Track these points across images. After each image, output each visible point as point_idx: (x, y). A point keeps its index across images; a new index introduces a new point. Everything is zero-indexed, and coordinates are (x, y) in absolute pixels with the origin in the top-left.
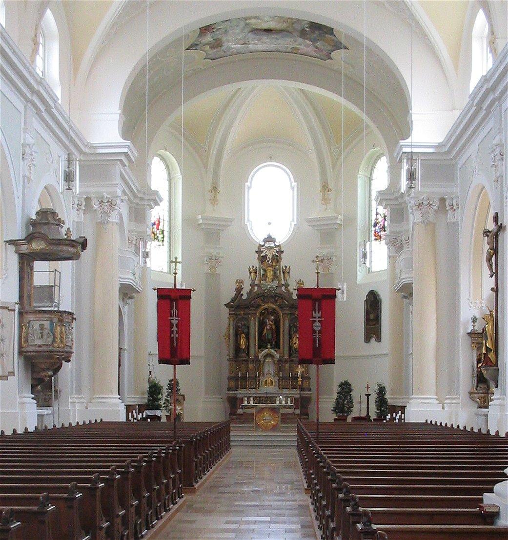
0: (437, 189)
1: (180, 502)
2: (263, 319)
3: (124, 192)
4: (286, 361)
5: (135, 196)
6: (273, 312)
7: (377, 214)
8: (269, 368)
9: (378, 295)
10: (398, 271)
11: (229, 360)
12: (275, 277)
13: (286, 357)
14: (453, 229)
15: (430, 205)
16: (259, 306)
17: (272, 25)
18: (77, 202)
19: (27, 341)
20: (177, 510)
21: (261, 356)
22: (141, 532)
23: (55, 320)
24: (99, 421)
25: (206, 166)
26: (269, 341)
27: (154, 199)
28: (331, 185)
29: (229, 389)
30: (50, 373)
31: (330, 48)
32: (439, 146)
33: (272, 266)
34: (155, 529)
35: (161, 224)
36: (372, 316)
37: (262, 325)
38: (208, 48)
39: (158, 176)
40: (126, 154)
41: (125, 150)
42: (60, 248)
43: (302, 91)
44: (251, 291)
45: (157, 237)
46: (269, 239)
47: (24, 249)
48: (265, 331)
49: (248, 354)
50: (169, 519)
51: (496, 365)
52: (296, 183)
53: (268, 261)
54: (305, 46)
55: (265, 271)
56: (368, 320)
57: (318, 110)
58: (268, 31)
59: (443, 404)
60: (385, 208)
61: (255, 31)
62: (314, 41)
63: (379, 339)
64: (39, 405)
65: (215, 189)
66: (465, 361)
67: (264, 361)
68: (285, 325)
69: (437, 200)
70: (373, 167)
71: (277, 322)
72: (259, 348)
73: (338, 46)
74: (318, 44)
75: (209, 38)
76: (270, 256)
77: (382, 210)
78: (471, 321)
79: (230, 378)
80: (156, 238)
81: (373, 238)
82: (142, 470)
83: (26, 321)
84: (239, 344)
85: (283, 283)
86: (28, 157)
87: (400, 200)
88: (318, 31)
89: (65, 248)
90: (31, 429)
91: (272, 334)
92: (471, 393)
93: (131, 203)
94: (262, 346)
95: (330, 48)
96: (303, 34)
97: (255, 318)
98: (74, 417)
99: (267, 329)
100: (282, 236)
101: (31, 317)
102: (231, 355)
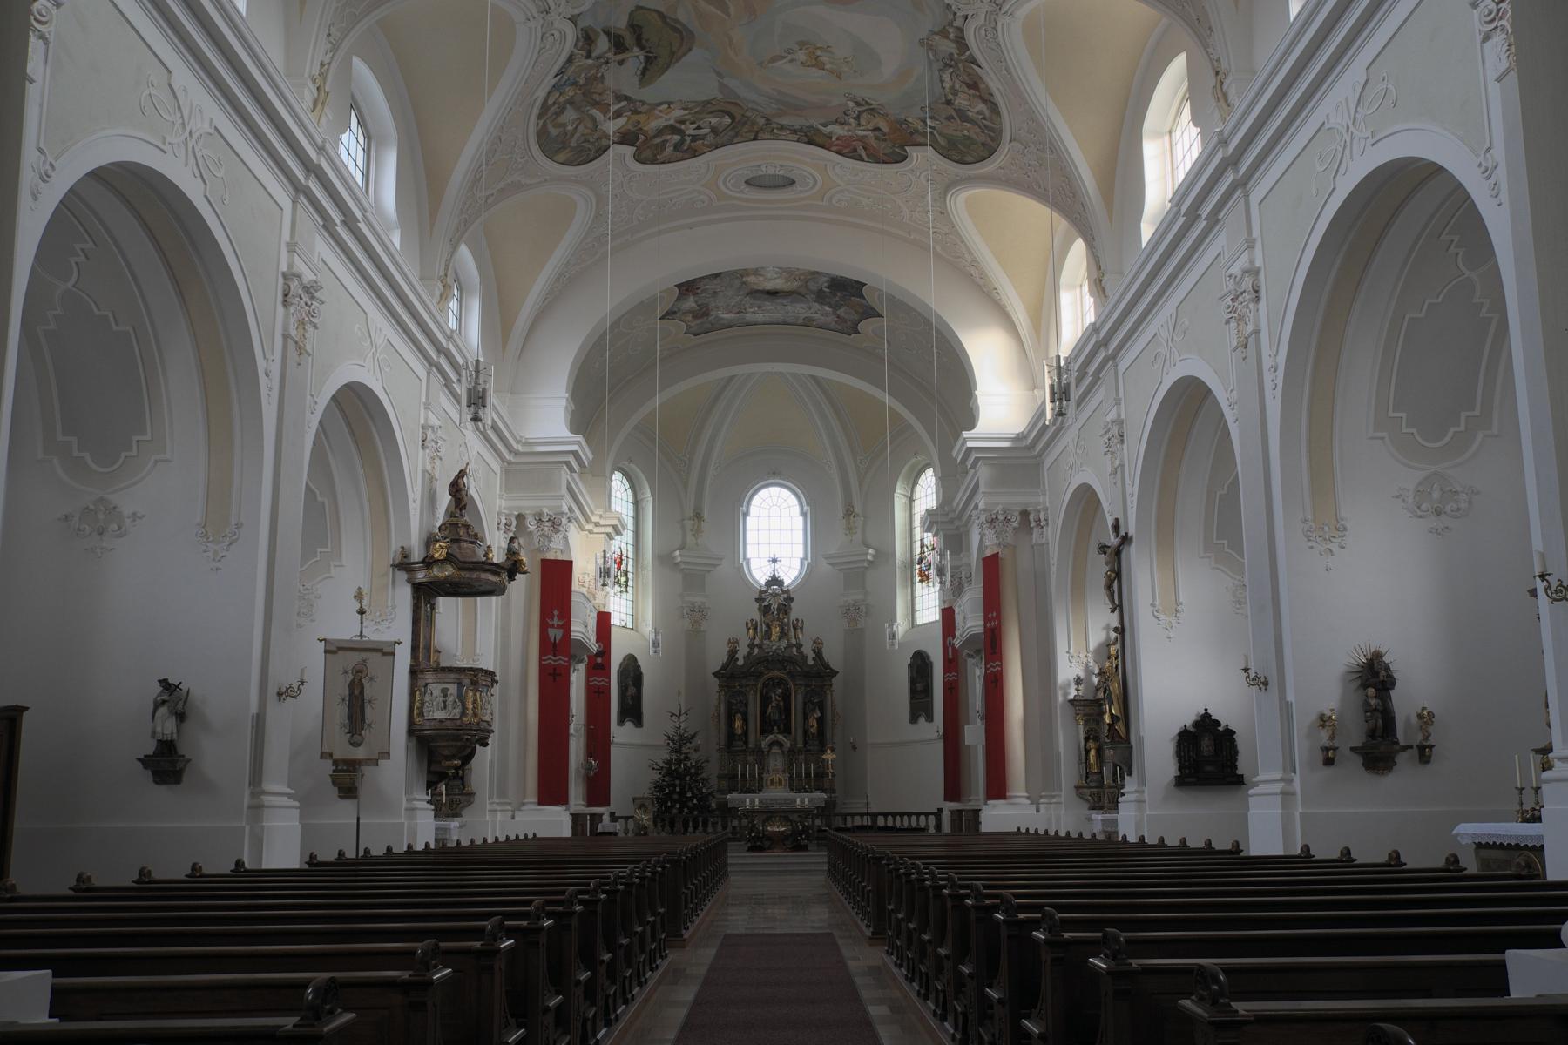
0: (1016, 499)
1: (663, 965)
4: (800, 751)
6: (780, 682)
7: (922, 546)
8: (776, 762)
11: (719, 751)
12: (783, 634)
13: (800, 745)
15: (1007, 520)
16: (761, 675)
17: (778, 284)
19: (421, 714)
20: (659, 983)
21: (764, 744)
22: (595, 1035)
23: (466, 682)
28: (858, 509)
31: (856, 317)
34: (620, 1026)
36: (919, 686)
37: (765, 701)
38: (689, 317)
40: (575, 454)
41: (575, 448)
42: (475, 575)
43: (814, 378)
44: (749, 654)
46: (774, 581)
47: (421, 576)
49: (746, 743)
50: (646, 1000)
51: (1128, 740)
54: (822, 313)
55: (768, 626)
56: (913, 692)
58: (773, 294)
59: (1038, 805)
61: (756, 293)
62: (835, 307)
64: (438, 814)
65: (698, 516)
66: (1067, 737)
68: (797, 701)
70: (915, 483)
71: (786, 697)
73: (870, 313)
74: (841, 312)
75: (690, 303)
76: (775, 605)
77: (929, 538)
80: (618, 583)
82: (599, 909)
83: (421, 683)
87: (957, 523)
88: (845, 296)
89: (484, 576)
90: (420, 847)
92: (1077, 788)
94: (766, 727)
95: (856, 317)
96: (820, 297)
98: (494, 830)
100: (790, 574)
101: (429, 677)
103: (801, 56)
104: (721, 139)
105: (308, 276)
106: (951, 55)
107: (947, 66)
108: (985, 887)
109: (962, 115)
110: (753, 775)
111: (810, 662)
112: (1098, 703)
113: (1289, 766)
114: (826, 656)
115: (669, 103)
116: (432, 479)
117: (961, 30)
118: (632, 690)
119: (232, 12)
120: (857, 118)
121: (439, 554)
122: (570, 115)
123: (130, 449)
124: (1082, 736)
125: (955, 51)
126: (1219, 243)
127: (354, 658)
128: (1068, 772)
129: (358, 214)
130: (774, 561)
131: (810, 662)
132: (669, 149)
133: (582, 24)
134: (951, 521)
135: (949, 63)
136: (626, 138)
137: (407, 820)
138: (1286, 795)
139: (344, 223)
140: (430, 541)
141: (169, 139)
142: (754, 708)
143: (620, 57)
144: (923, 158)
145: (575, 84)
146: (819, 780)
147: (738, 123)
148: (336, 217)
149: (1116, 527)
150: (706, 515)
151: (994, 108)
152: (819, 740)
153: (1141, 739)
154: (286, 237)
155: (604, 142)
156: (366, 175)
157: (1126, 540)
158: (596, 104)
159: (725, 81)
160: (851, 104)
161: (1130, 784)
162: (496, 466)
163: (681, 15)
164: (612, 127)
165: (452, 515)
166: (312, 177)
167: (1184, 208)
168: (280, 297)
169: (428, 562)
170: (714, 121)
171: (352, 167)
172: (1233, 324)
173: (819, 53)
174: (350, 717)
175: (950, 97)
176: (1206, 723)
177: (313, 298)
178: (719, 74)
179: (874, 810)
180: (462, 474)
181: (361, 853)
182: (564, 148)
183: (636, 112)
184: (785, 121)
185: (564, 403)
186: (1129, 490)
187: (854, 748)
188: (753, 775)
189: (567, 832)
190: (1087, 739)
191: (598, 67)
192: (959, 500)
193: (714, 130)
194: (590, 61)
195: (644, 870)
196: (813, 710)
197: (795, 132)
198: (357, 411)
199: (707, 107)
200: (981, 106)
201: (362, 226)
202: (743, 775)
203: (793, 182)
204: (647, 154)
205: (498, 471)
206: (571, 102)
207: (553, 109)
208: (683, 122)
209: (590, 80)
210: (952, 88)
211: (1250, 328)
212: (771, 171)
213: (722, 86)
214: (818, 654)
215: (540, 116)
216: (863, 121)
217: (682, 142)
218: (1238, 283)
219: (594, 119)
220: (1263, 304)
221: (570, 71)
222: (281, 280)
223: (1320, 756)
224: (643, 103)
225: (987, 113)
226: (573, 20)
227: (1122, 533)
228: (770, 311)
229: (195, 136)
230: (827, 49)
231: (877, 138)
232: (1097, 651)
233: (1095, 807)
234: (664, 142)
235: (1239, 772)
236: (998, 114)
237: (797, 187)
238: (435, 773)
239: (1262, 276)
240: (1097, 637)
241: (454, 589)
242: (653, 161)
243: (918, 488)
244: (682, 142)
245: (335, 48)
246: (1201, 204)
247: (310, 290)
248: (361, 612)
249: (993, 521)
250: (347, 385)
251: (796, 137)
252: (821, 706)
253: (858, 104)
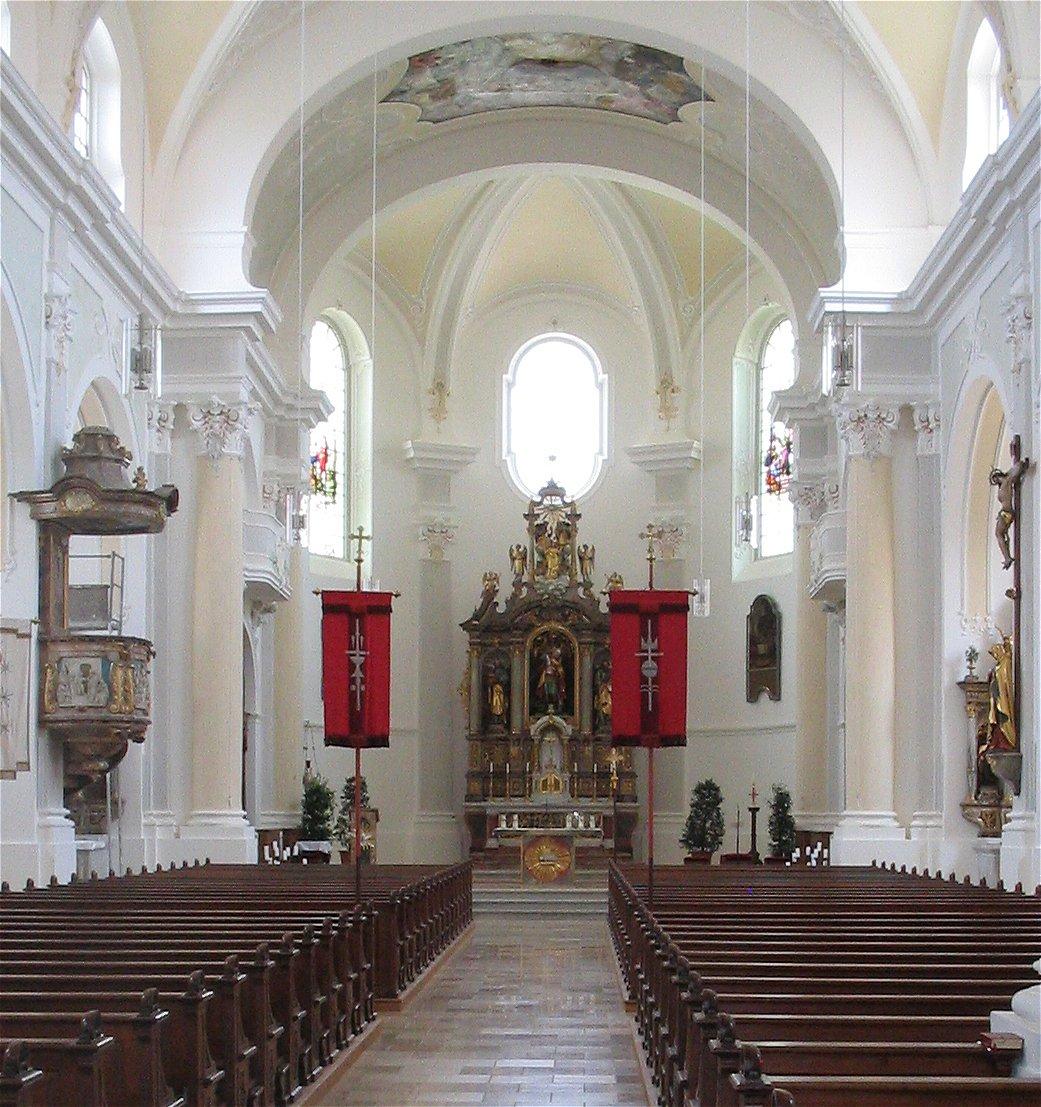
0: (896, 388)
1: (369, 1028)
2: (539, 655)
3: (253, 393)
4: (586, 740)
5: (277, 402)
6: (560, 639)
7: (773, 438)
8: (552, 754)
9: (775, 604)
10: (815, 556)
11: (469, 738)
12: (564, 567)
13: (587, 732)
14: (928, 470)
15: (881, 419)
16: (530, 627)
17: (557, 51)
18: (157, 415)
19: (55, 699)
20: (364, 1046)
21: (534, 729)
23: (114, 656)
24: (202, 863)
25: (421, 341)
26: (552, 700)
27: (316, 408)
28: (678, 380)
29: (470, 798)
31: (675, 98)
32: (900, 299)
33: (557, 545)
34: (317, 1085)
35: (330, 459)
36: (762, 649)
37: (537, 665)
38: (425, 98)
39: (324, 361)
40: (257, 315)
41: (257, 308)
42: (123, 508)
43: (619, 186)
44: (515, 596)
45: (322, 485)
46: (552, 490)
47: (49, 510)
48: (543, 679)
49: (508, 726)
50: (347, 1065)
51: (1017, 748)
52: (606, 376)
53: (550, 536)
54: (625, 93)
55: (543, 555)
56: (753, 656)
57: (653, 225)
58: (550, 63)
59: (908, 828)
60: (788, 426)
61: (522, 63)
62: (644, 83)
63: (776, 695)
64: (81, 831)
65: (440, 387)
66: (952, 740)
67: (541, 740)
69: (895, 411)
70: (764, 343)
71: (567, 661)
72: (531, 713)
73: (692, 94)
74: (652, 91)
75: (427, 78)
76: (553, 525)
77: (782, 431)
78: (965, 658)
79: (471, 776)
80: (320, 488)
81: (765, 487)
82: (292, 964)
83: (52, 657)
84: (490, 705)
85: (580, 579)
86: (57, 322)
88: (652, 64)
89: (134, 509)
90: (64, 880)
91: (557, 684)
92: (964, 806)
93: (269, 415)
94: (536, 710)
95: (675, 98)
96: (621, 69)
97: (522, 652)
98: (152, 856)
99: (547, 674)
100: (577, 485)
101: (64, 650)
102: (474, 728)
108: (683, 946)
134: (812, 407)
195: (358, 914)
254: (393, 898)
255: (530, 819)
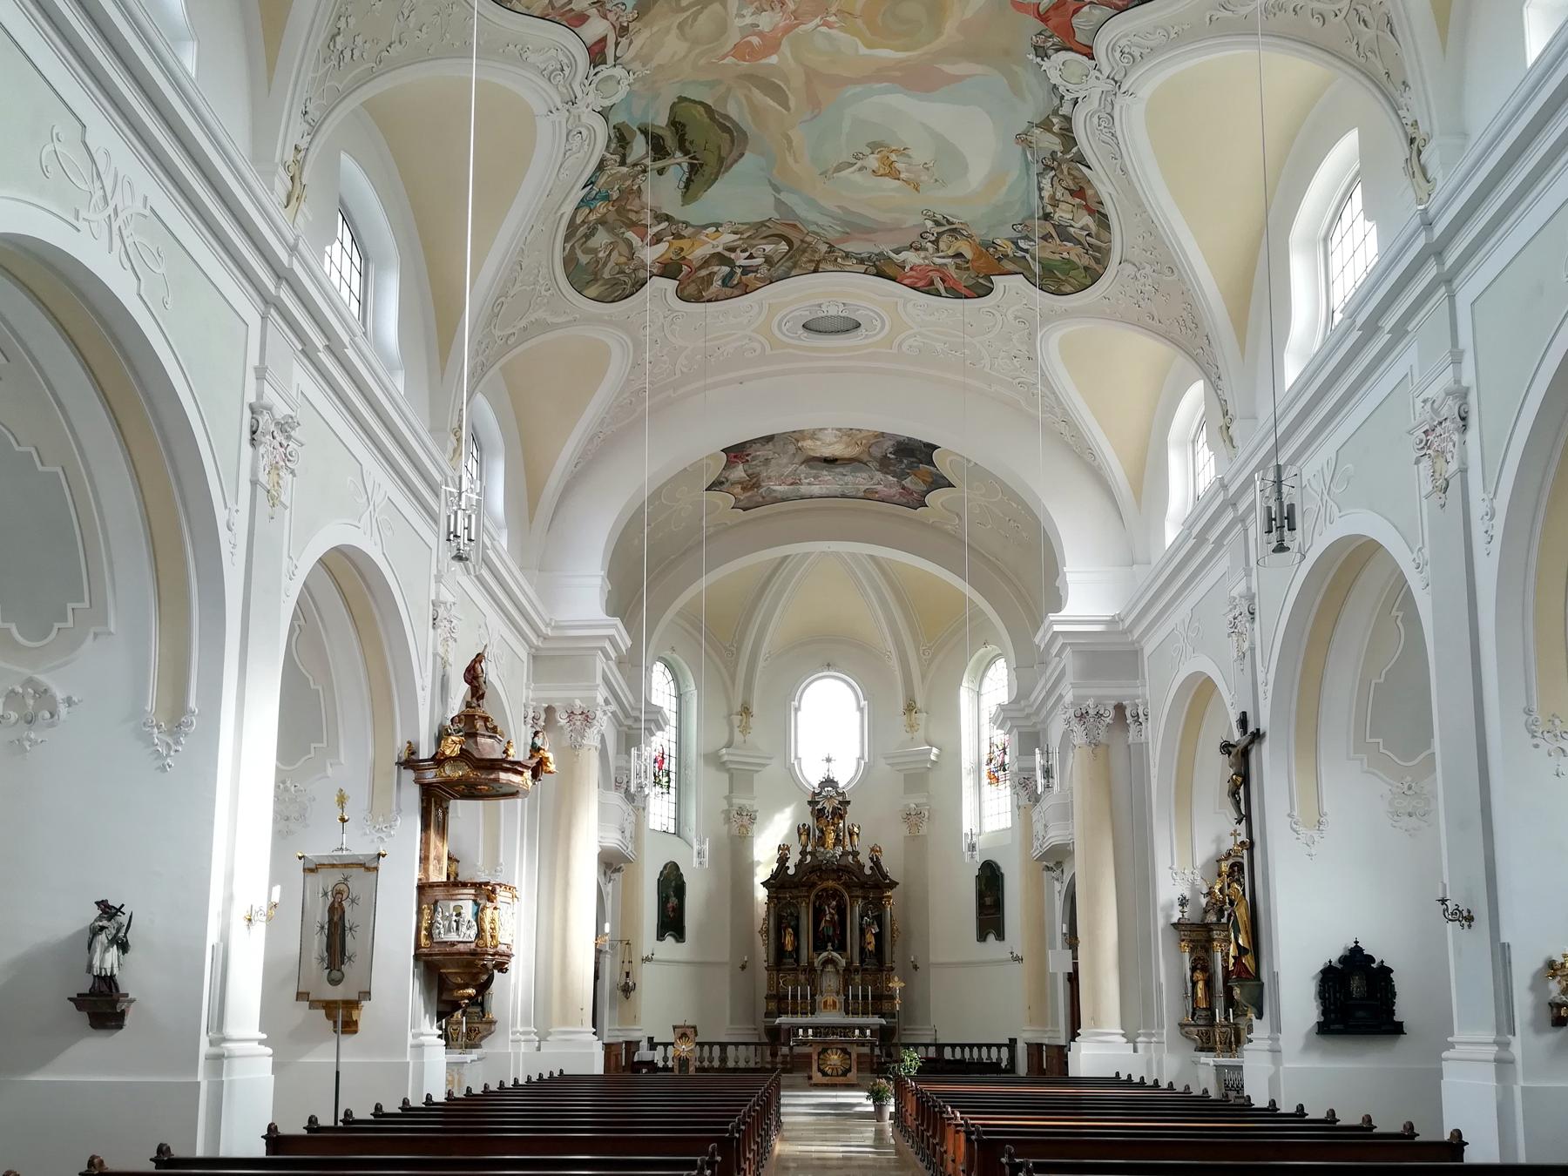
0: (1110, 691)
3: (607, 702)
4: (856, 970)
5: (627, 716)
6: (835, 894)
8: (830, 982)
10: (1038, 827)
12: (838, 841)
14: (1138, 755)
16: (814, 885)
17: (837, 450)
18: (531, 715)
19: (430, 936)
24: (556, 1074)
26: (830, 939)
27: (655, 720)
29: (768, 1015)
30: (471, 991)
32: (1112, 621)
36: (988, 901)
37: (818, 914)
38: (738, 489)
39: (661, 688)
40: (611, 639)
44: (801, 861)
46: (829, 782)
47: (430, 776)
49: (797, 960)
51: (1257, 977)
54: (885, 483)
55: (822, 831)
57: (902, 592)
58: (831, 461)
59: (1135, 1043)
60: (1009, 732)
61: (812, 461)
62: (901, 476)
63: (1000, 936)
65: (746, 710)
66: (1168, 967)
69: (1111, 709)
72: (815, 950)
74: (907, 482)
75: (739, 472)
76: (829, 808)
77: (1000, 737)
78: (1177, 903)
81: (985, 781)
85: (849, 848)
86: (443, 624)
88: (911, 462)
89: (503, 776)
93: (621, 725)
94: (819, 946)
96: (884, 464)
100: (844, 775)
103: (873, 162)
104: (778, 271)
105: (282, 410)
106: (1054, 153)
107: (1048, 168)
109: (1063, 233)
110: (804, 997)
111: (868, 871)
112: (1206, 928)
113: (1506, 1024)
114: (886, 868)
115: (717, 225)
116: (445, 664)
117: (1068, 119)
118: (673, 901)
119: (180, 75)
120: (936, 242)
121: (452, 748)
122: (601, 238)
123: (65, 620)
124: (1188, 965)
125: (1058, 148)
126: (1407, 359)
127: (330, 879)
128: (1169, 1002)
129: (346, 339)
130: (829, 760)
131: (868, 871)
132: (717, 283)
133: (616, 119)
134: (1028, 716)
135: (1050, 165)
136: (669, 270)
137: (417, 1062)
138: (1503, 1064)
139: (327, 347)
140: (441, 735)
141: (83, 214)
142: (806, 922)
143: (660, 164)
144: (1010, 287)
145: (607, 198)
146: (879, 1001)
147: (795, 250)
148: (318, 340)
149: (1243, 722)
150: (755, 709)
151: (1103, 220)
152: (877, 961)
153: (1275, 977)
154: (253, 359)
155: (642, 274)
156: (362, 303)
157: (1257, 736)
158: (632, 225)
159: (783, 196)
160: (929, 224)
161: (1261, 1029)
162: (523, 653)
163: (732, 110)
164: (650, 254)
165: (468, 705)
166: (284, 285)
167: (1361, 319)
168: (247, 435)
169: (438, 760)
170: (768, 248)
171: (345, 293)
172: (1426, 462)
173: (893, 157)
174: (329, 947)
175: (1049, 209)
176: (1356, 959)
177: (289, 438)
178: (777, 189)
179: (941, 1041)
180: (479, 658)
181: (341, 1116)
182: (596, 280)
183: (678, 236)
184: (850, 247)
185: (599, 581)
186: (1260, 677)
187: (916, 968)
188: (804, 997)
189: (598, 1068)
190: (1193, 970)
191: (635, 177)
192: (1038, 694)
193: (768, 260)
194: (624, 169)
196: (869, 925)
197: (861, 261)
198: (348, 580)
199: (761, 230)
200: (1087, 220)
201: (350, 352)
202: (794, 996)
203: (858, 325)
204: (691, 289)
205: (525, 658)
206: (602, 221)
207: (583, 230)
208: (732, 250)
209: (626, 194)
210: (1053, 197)
211: (1454, 466)
212: (833, 311)
213: (779, 204)
214: (876, 864)
215: (567, 239)
216: (942, 246)
217: (732, 274)
218: (1436, 412)
219: (630, 245)
220: (1473, 434)
221: (602, 181)
222: (247, 414)
223: (1547, 1016)
224: (687, 224)
225: (1093, 228)
226: (604, 113)
227: (1251, 729)
228: (829, 482)
229: (122, 216)
230: (903, 152)
231: (958, 267)
232: (1205, 866)
233: (1206, 1046)
234: (712, 274)
235: (1396, 1019)
236: (1107, 228)
237: (862, 329)
238: (445, 1002)
239: (1472, 398)
240: (1205, 850)
241: (470, 791)
242: (698, 299)
243: (986, 681)
244: (732, 274)
245: (314, 130)
246: (1375, 325)
247: (285, 426)
248: (343, 820)
249: (1082, 717)
250: (336, 549)
251: (862, 268)
252: (879, 920)
253: (937, 223)
254: (732, 1133)
255: (817, 1029)
